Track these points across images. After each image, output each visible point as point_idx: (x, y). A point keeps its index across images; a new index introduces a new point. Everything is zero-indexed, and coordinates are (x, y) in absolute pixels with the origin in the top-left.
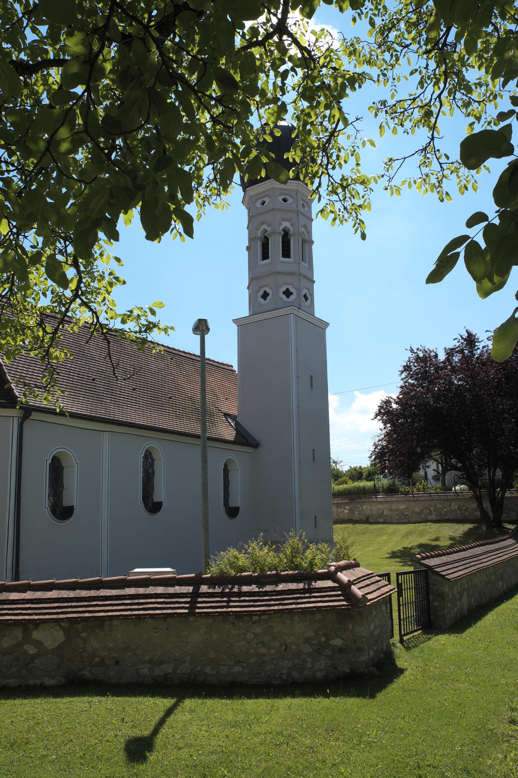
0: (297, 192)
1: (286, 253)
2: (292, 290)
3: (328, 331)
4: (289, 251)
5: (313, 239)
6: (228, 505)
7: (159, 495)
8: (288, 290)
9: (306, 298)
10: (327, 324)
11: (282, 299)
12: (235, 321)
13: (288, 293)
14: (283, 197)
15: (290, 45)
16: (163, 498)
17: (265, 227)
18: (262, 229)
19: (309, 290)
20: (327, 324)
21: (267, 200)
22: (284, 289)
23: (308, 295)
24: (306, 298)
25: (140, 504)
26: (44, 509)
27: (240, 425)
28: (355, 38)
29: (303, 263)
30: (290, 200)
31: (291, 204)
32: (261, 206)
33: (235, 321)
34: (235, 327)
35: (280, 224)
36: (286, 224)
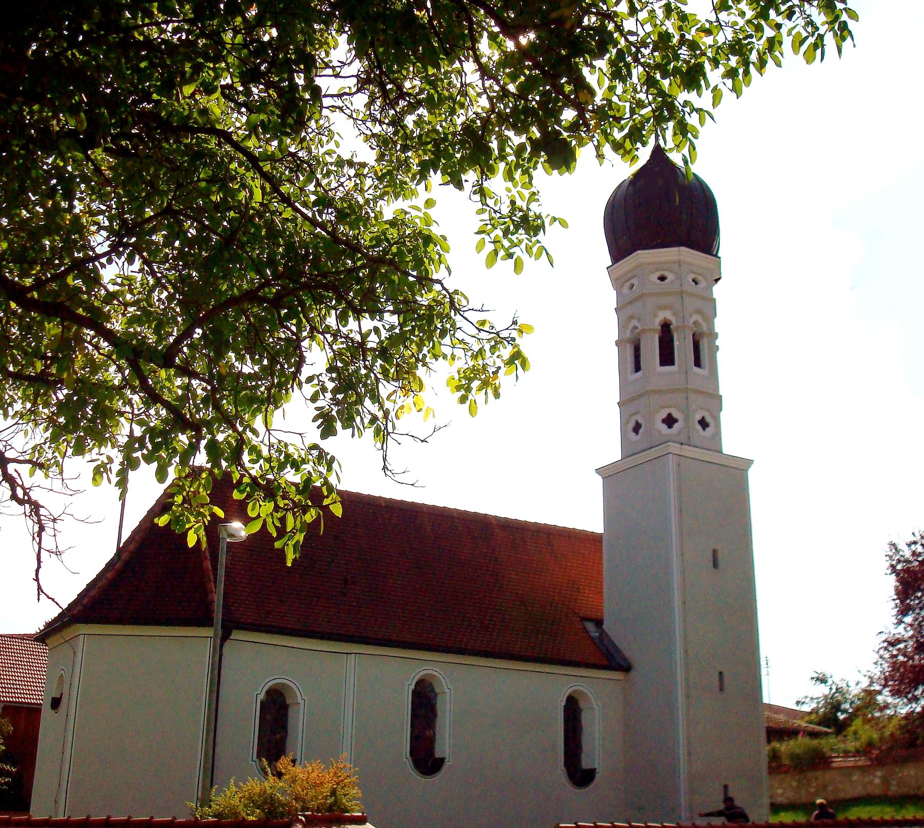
0: (679, 263)
1: (667, 357)
2: (676, 415)
3: (752, 474)
4: (672, 354)
5: (716, 330)
6: (580, 765)
7: (444, 746)
8: (670, 415)
9: (704, 424)
10: (750, 462)
11: (659, 431)
12: (598, 471)
13: (670, 421)
14: (658, 274)
15: (273, 168)
16: (447, 752)
17: (634, 322)
18: (631, 326)
19: (708, 410)
20: (750, 462)
21: (635, 281)
22: (664, 416)
23: (708, 419)
24: (704, 424)
25: (405, 759)
26: (251, 762)
27: (607, 635)
28: (707, 20)
29: (697, 370)
30: (670, 277)
31: (672, 282)
32: (629, 291)
33: (598, 471)
34: (599, 480)
35: (655, 315)
36: (666, 315)
